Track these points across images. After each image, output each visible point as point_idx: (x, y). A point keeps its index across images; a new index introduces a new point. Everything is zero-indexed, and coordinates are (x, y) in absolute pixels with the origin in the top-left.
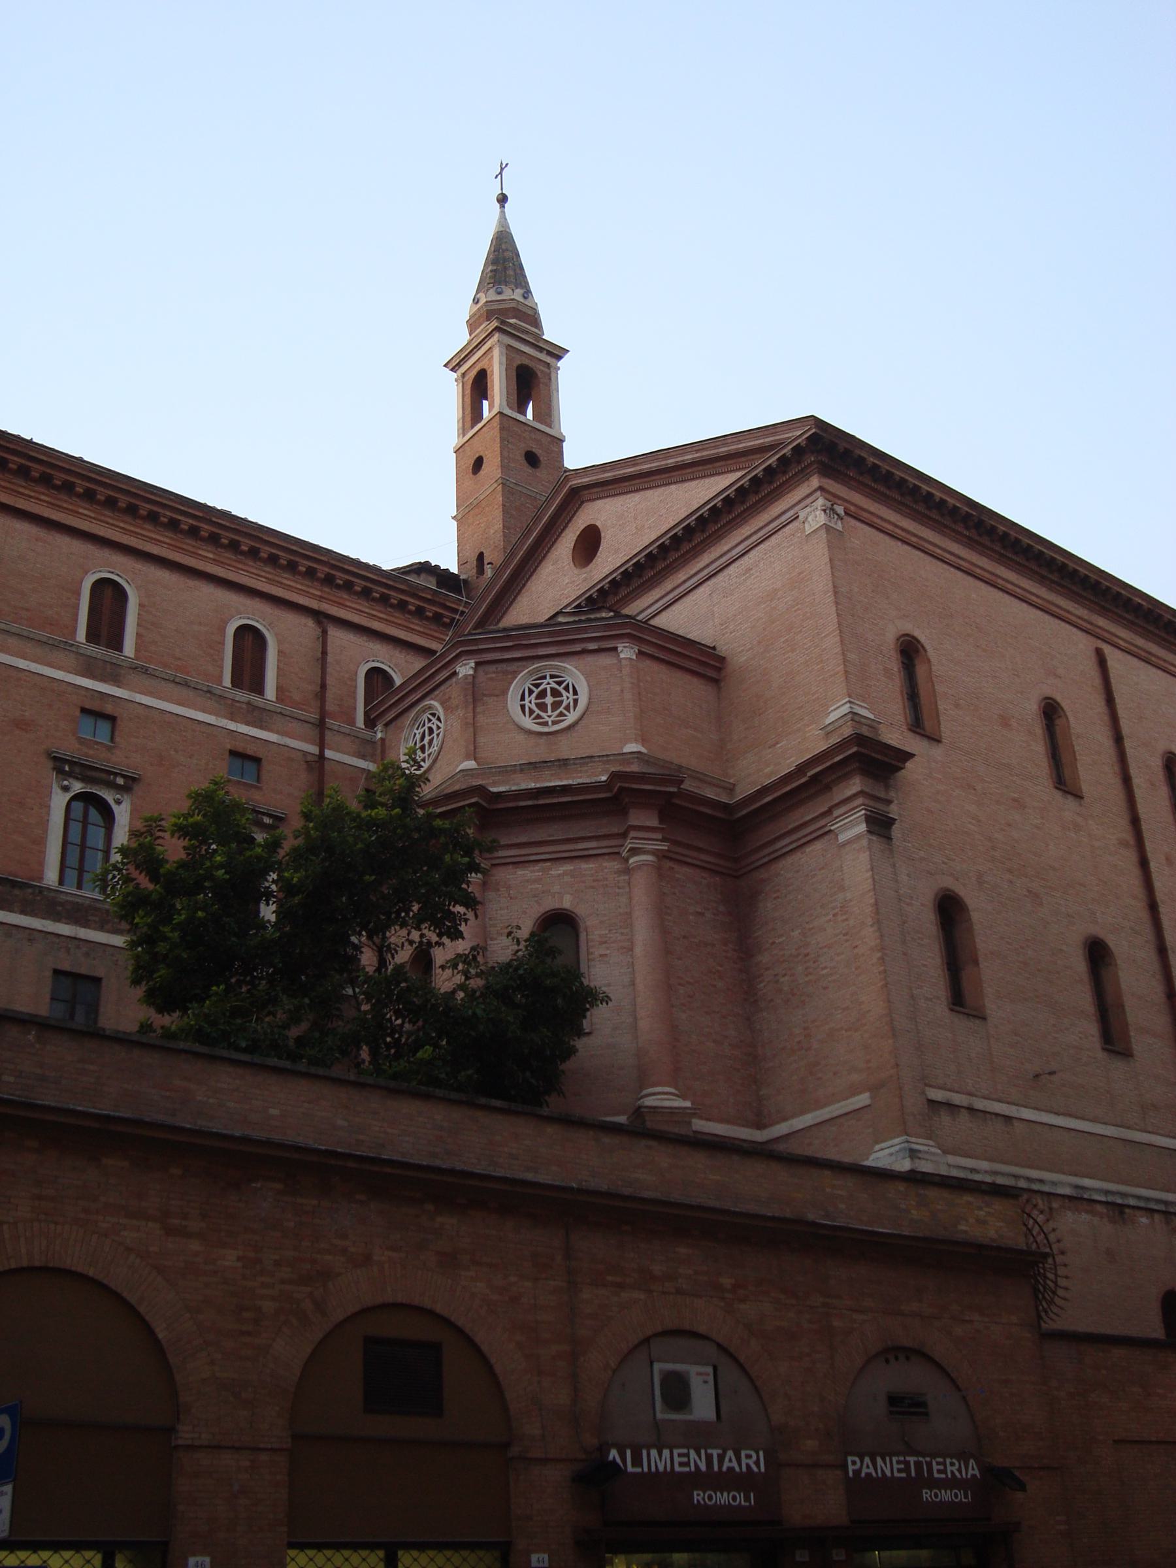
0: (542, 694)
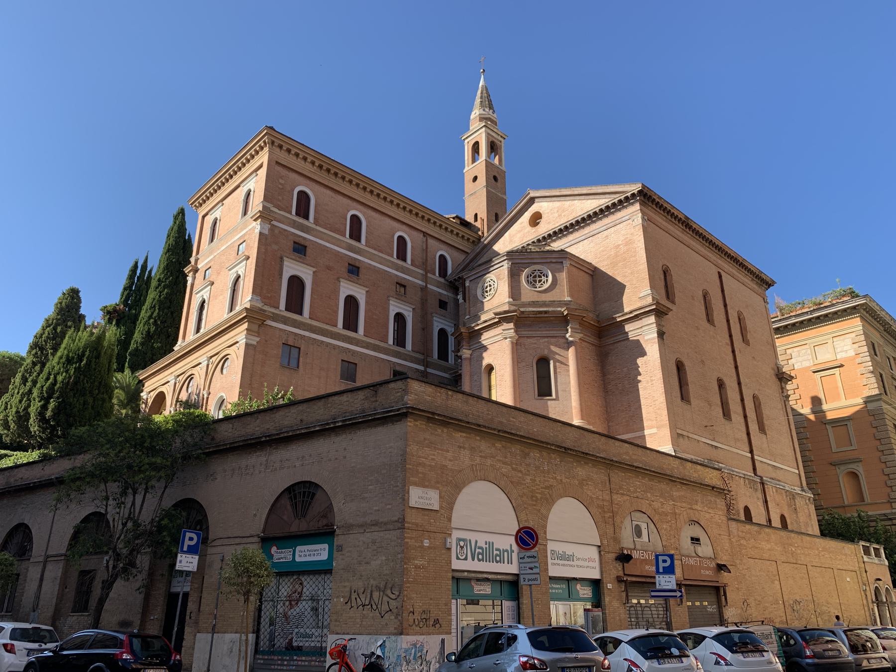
0: (535, 277)
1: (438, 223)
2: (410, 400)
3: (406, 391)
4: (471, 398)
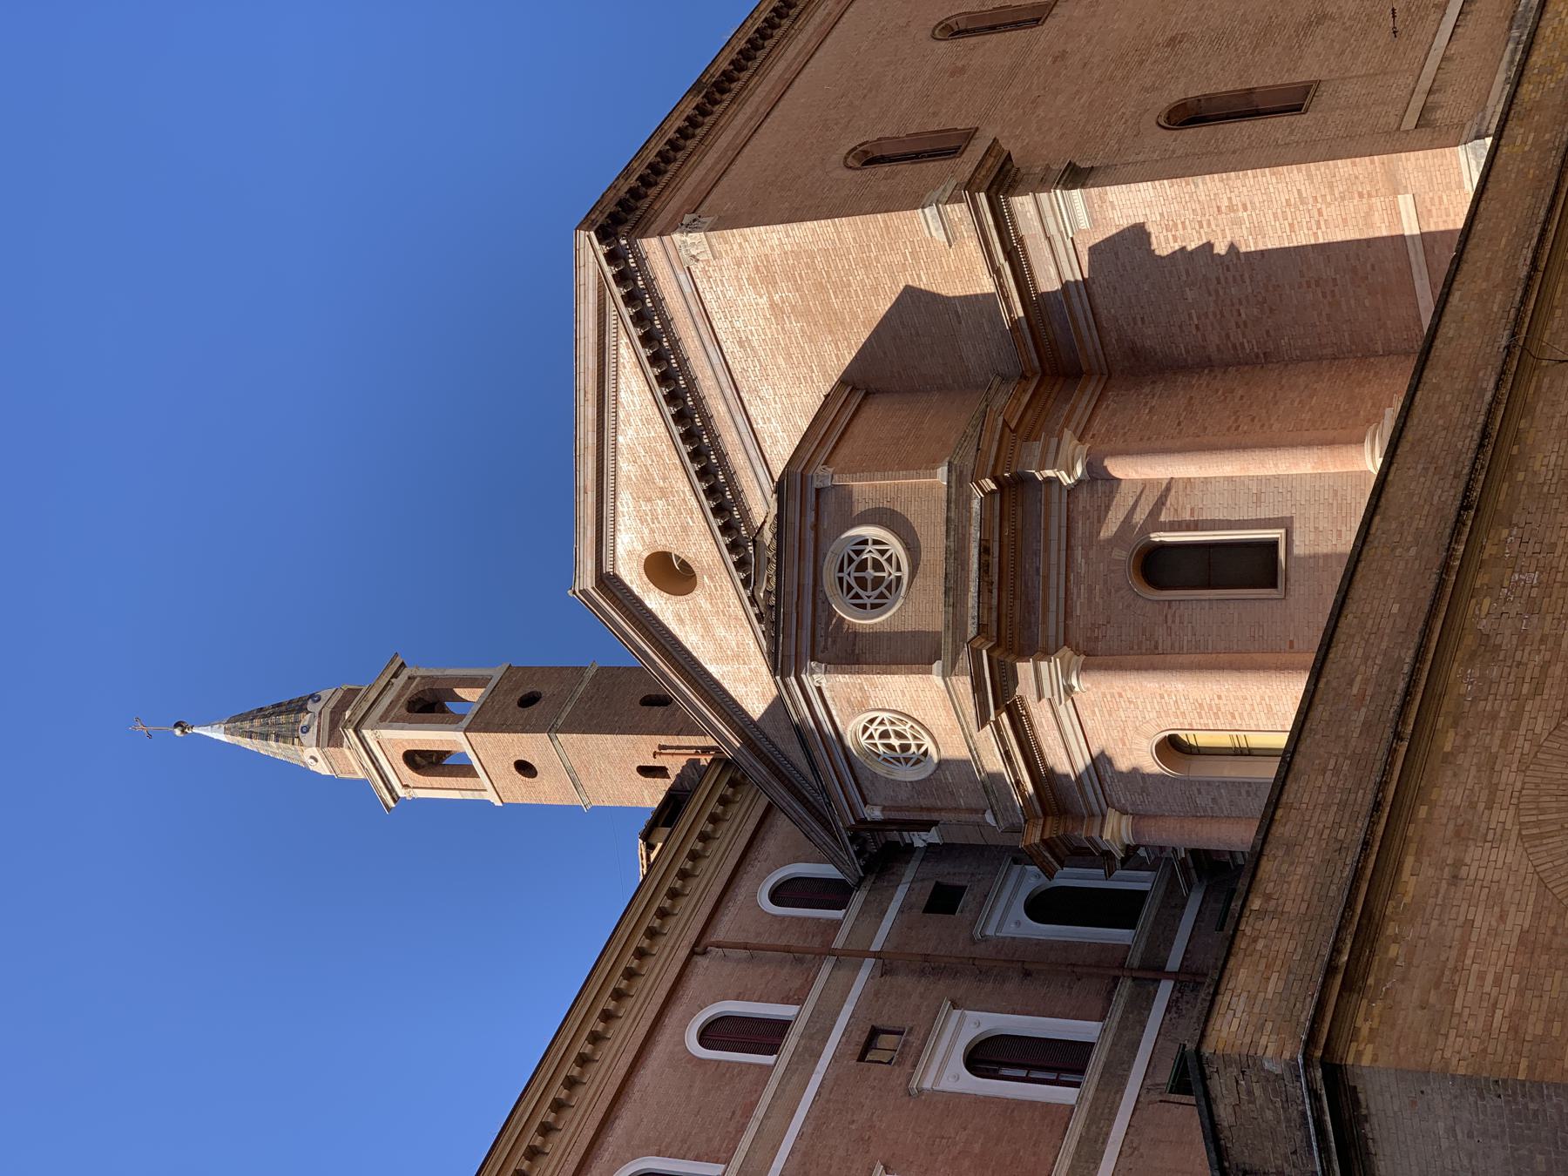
0: (862, 582)
1: (663, 901)
2: (1278, 1049)
3: (1248, 1064)
4: (1277, 830)
